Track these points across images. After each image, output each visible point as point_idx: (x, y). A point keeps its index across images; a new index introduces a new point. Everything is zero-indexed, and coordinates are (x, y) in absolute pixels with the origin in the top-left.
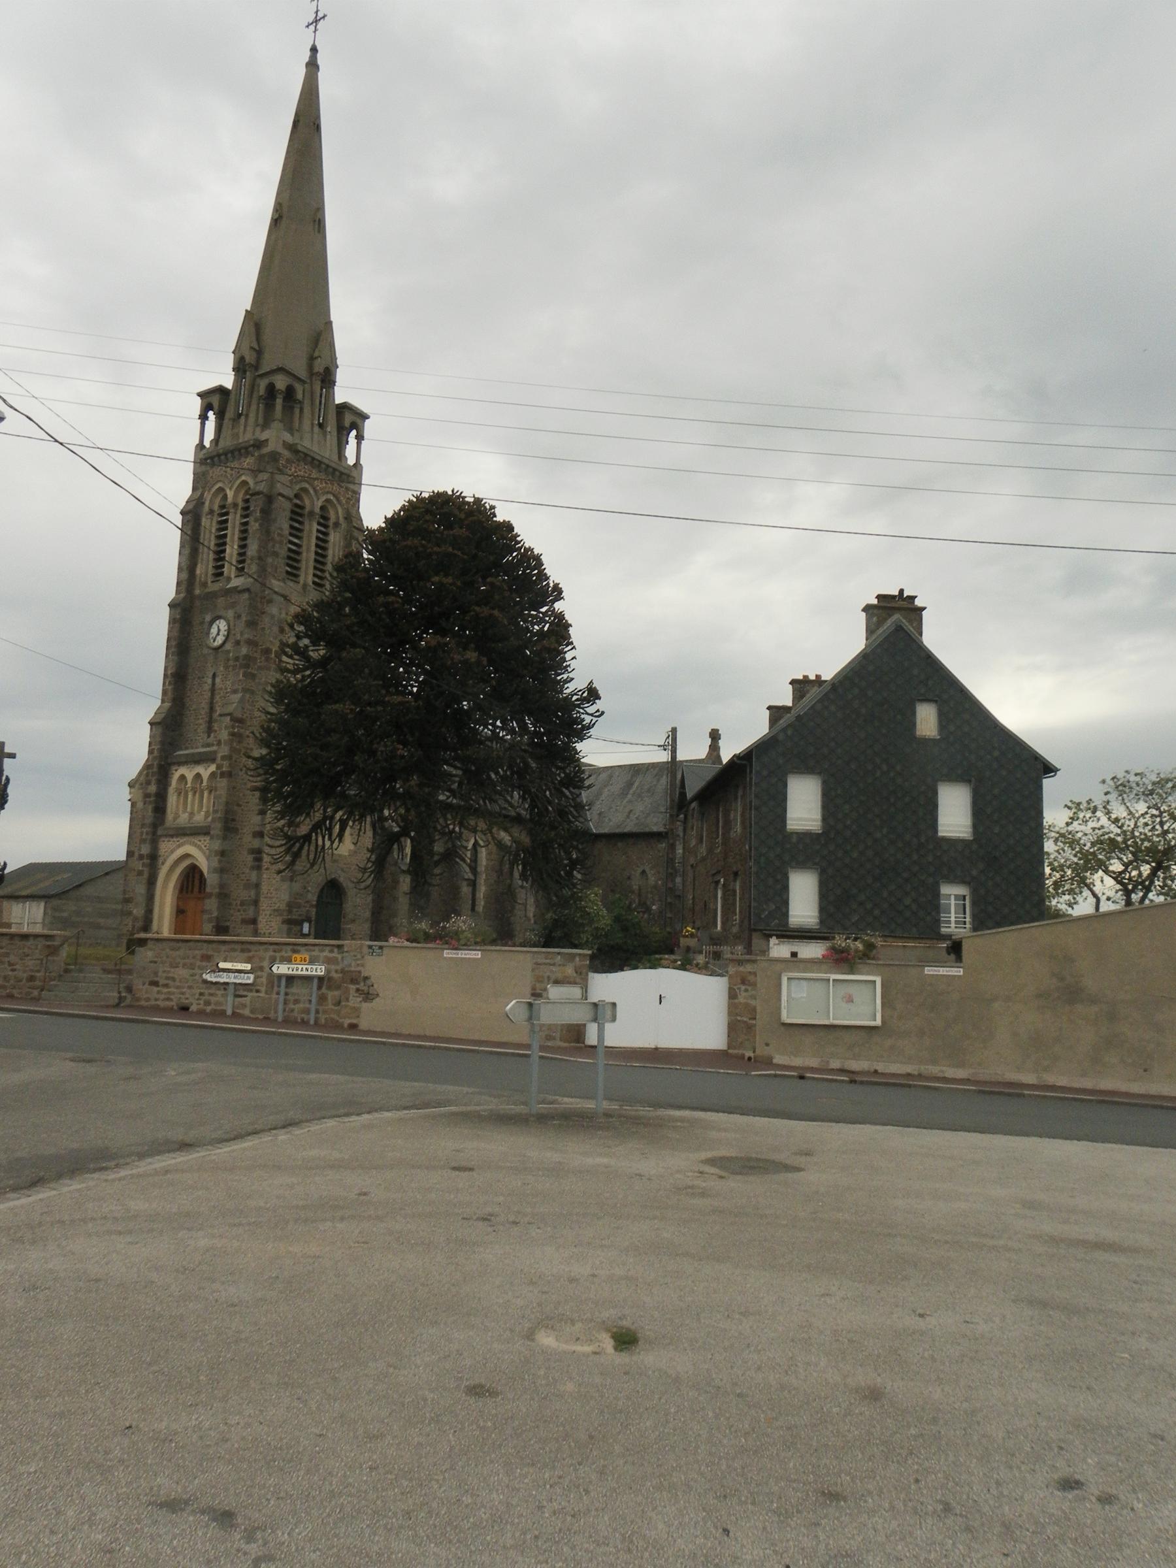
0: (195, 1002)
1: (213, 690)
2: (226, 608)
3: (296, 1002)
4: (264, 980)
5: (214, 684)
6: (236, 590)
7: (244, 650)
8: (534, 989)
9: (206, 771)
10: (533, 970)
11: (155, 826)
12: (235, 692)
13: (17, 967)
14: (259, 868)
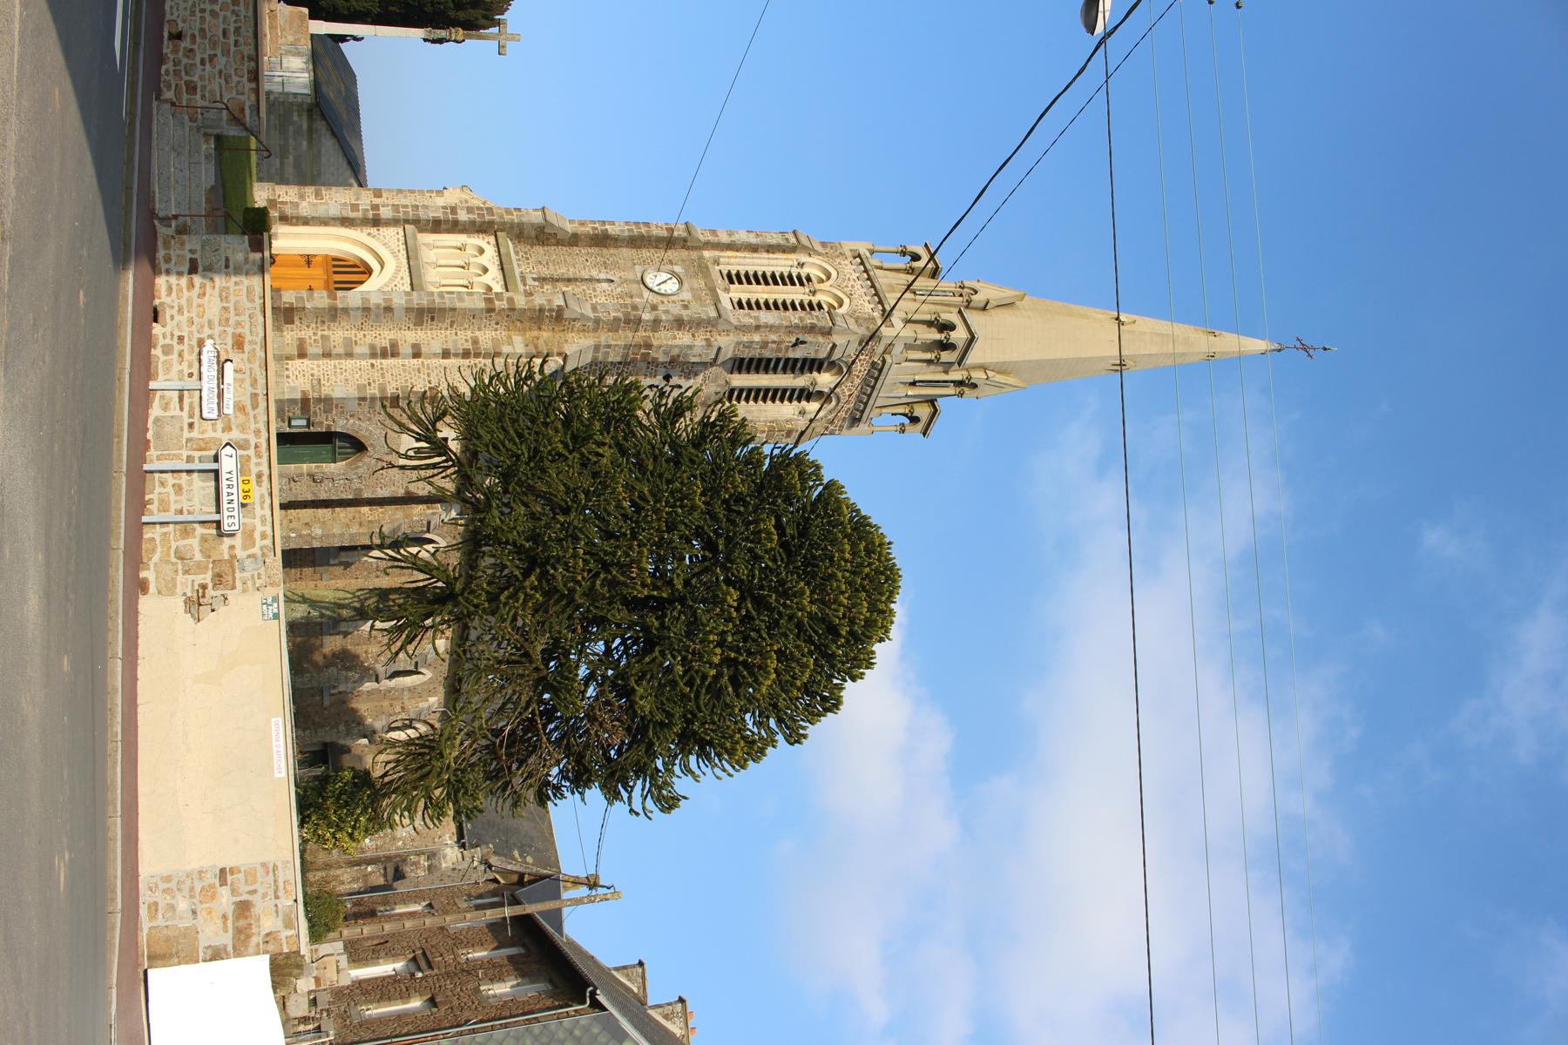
0: (168, 330)
1: (591, 280)
2: (692, 289)
3: (178, 489)
4: (210, 434)
5: (599, 281)
6: (716, 303)
7: (646, 316)
8: (232, 871)
9: (494, 279)
10: (264, 865)
11: (416, 222)
12: (594, 308)
13: (208, 67)
14: (373, 355)
